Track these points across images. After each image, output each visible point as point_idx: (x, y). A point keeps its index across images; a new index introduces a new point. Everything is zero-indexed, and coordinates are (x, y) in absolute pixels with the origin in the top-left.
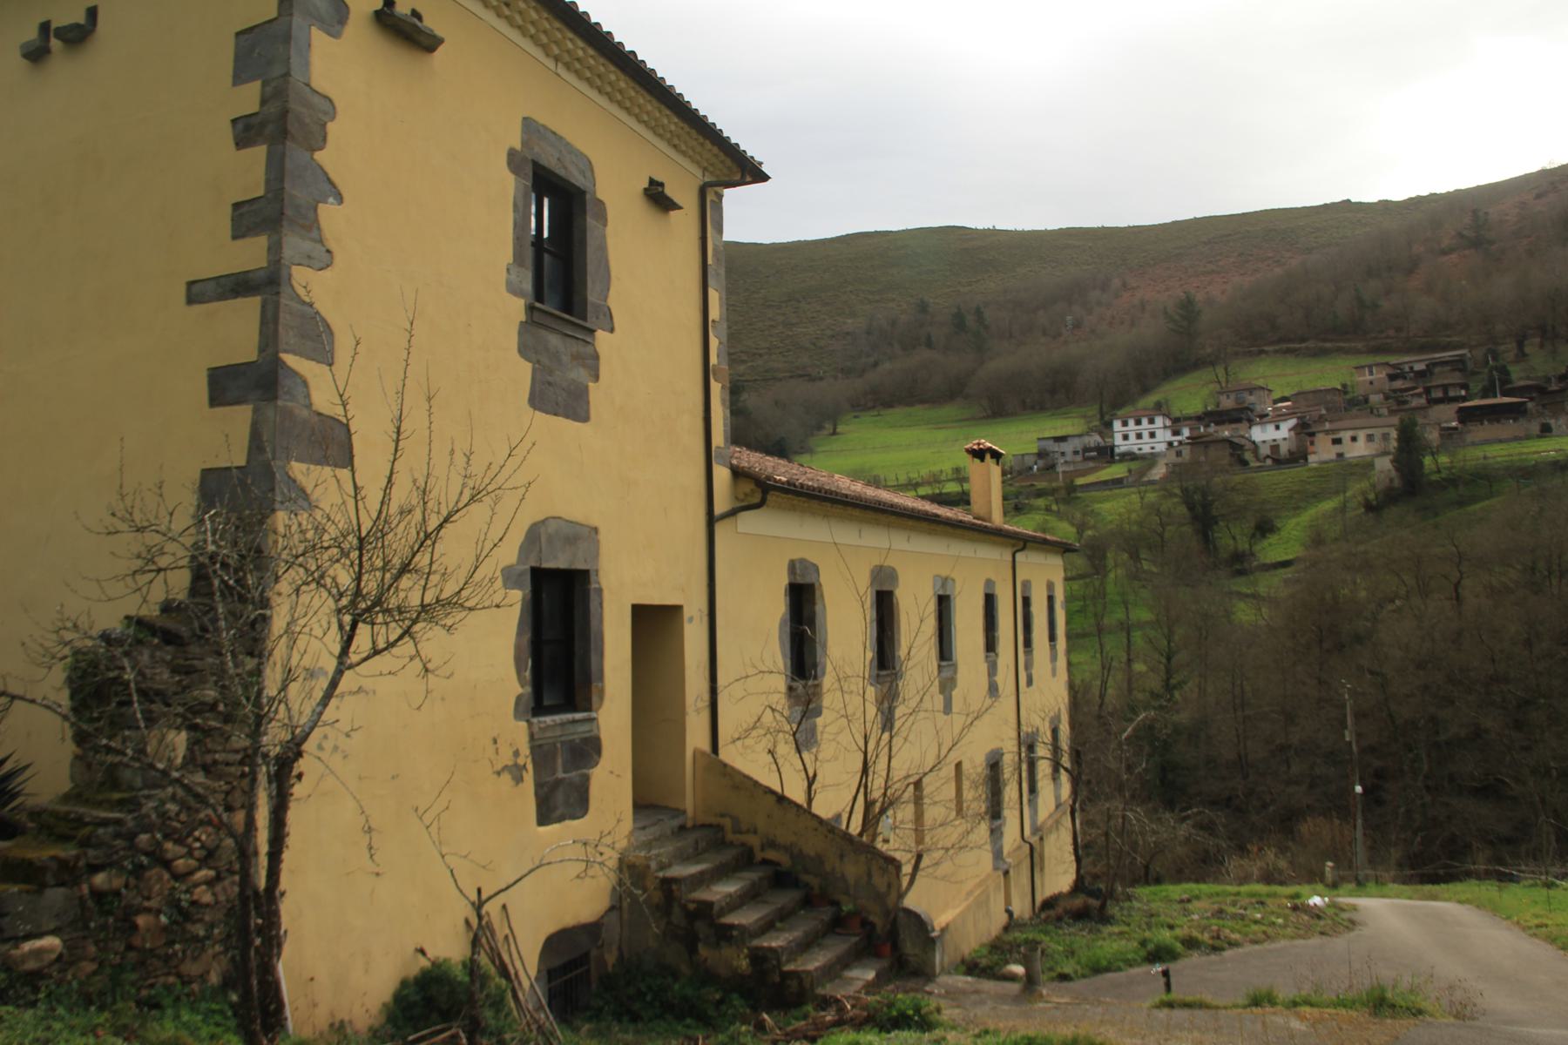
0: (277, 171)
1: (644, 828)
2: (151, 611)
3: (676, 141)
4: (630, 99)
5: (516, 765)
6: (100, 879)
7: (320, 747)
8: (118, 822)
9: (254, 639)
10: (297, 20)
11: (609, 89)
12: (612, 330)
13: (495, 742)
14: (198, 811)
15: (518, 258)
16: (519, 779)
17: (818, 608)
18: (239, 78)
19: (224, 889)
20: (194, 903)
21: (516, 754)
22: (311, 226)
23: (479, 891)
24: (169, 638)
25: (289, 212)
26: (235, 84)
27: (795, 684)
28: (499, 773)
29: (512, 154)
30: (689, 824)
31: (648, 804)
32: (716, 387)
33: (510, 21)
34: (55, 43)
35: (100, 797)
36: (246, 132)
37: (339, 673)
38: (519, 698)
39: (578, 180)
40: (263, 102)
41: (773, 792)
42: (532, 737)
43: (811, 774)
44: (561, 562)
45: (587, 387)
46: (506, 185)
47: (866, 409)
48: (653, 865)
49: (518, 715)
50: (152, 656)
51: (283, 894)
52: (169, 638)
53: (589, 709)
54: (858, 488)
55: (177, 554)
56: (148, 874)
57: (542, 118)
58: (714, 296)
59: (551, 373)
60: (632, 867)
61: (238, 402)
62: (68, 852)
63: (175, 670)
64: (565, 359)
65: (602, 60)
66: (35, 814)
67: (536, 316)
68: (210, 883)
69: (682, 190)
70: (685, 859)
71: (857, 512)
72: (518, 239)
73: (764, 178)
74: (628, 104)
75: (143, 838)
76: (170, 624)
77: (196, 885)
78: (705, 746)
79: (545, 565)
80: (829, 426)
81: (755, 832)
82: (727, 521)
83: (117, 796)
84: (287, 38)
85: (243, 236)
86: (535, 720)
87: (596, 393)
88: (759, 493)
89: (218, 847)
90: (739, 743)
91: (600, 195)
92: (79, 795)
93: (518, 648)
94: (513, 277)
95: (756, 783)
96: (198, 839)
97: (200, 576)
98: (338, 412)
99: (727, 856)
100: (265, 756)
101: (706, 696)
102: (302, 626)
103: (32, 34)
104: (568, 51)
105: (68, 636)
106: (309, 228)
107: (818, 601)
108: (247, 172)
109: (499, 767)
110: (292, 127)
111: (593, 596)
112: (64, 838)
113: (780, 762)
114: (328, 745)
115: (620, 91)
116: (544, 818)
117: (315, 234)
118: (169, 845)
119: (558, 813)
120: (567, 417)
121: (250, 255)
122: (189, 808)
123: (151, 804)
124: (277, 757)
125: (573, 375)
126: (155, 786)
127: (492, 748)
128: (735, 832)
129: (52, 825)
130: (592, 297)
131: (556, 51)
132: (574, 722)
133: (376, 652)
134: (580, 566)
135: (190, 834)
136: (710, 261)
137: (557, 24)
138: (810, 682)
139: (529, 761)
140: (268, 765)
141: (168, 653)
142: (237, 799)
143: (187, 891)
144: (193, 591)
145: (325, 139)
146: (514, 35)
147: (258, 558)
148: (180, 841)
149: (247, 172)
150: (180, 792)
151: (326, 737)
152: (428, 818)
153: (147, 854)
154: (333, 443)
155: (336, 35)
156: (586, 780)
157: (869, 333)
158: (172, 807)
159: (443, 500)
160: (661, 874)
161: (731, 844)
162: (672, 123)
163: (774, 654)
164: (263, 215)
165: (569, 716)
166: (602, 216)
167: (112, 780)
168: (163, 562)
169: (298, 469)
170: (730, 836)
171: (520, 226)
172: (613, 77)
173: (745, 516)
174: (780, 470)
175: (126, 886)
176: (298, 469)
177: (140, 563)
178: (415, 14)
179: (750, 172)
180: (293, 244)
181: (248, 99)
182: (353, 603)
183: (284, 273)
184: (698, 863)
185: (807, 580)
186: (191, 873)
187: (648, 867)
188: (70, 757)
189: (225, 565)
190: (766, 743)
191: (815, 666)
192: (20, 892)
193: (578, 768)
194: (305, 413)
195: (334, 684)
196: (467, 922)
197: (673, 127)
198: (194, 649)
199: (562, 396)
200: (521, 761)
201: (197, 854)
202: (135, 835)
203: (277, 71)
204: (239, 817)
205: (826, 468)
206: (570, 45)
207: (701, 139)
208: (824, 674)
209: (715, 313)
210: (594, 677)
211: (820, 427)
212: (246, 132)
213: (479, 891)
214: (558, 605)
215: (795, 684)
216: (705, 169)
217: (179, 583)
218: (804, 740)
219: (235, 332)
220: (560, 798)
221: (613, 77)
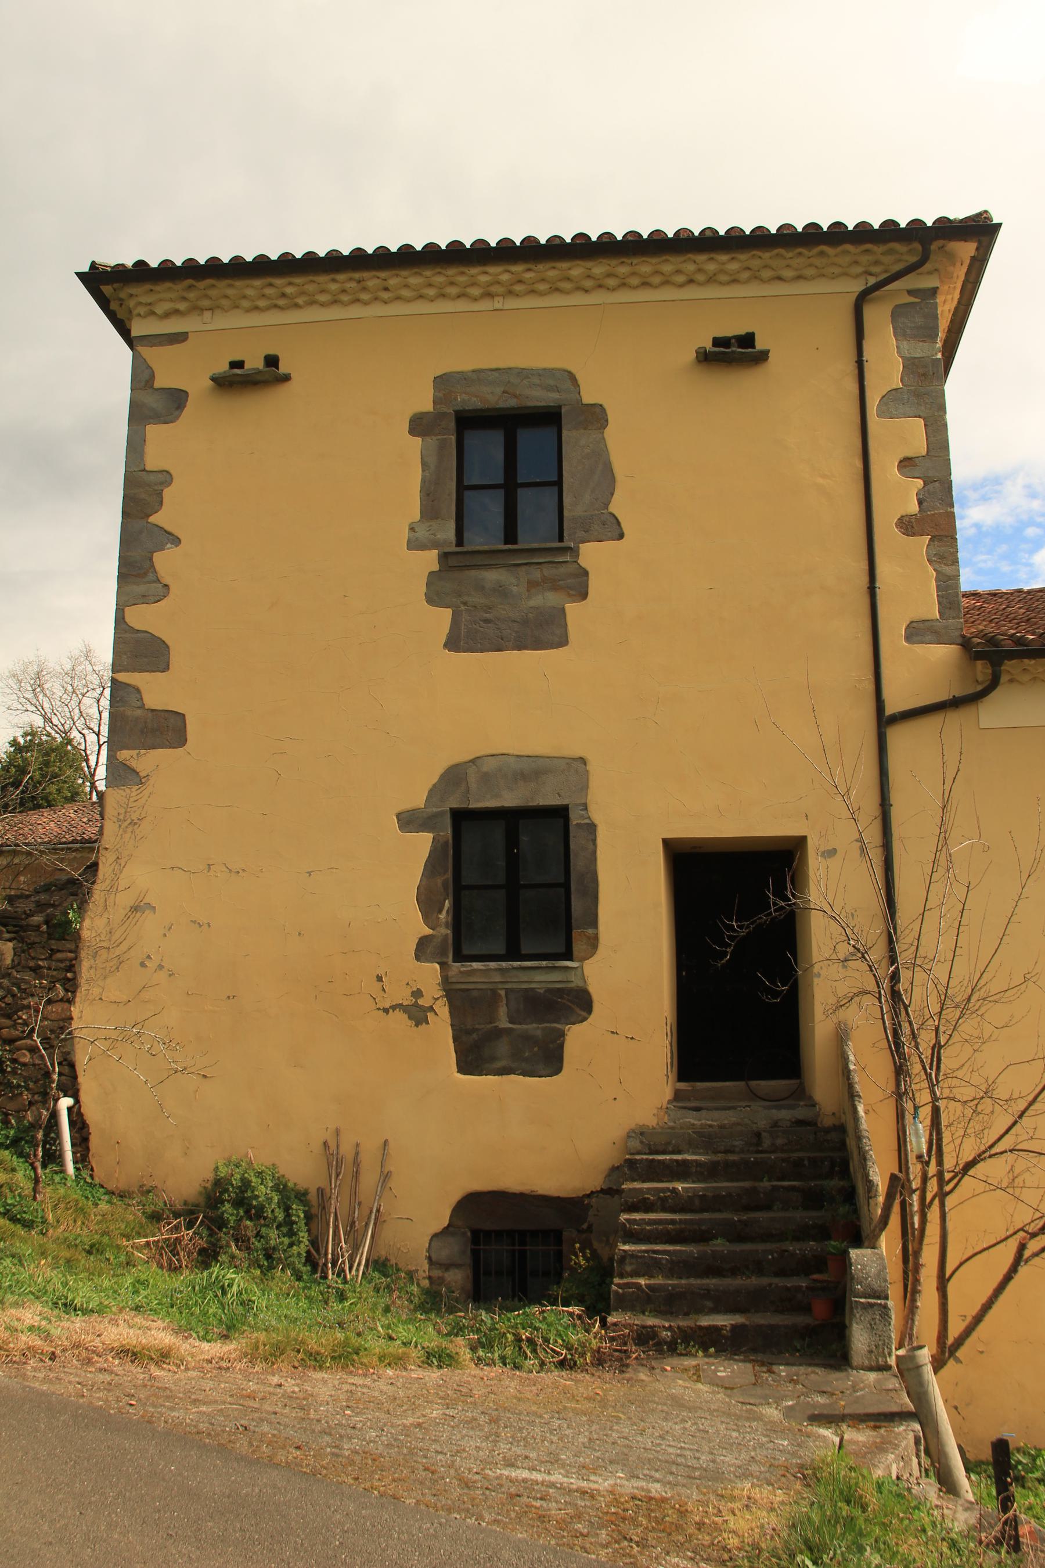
13: (380, 979)
15: (430, 511)
45: (563, 609)
77: (19, 1049)
79: (474, 805)
117: (151, 576)
135: (16, 1013)
156: (560, 1036)
194: (139, 712)
196: (325, 1143)
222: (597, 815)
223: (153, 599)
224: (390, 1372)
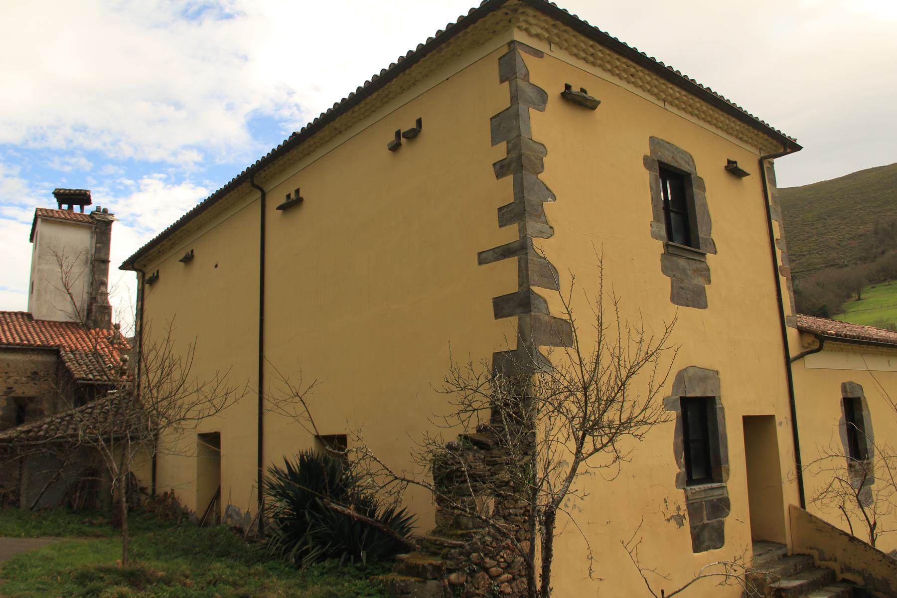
0: (519, 188)
1: (760, 555)
2: (472, 432)
3: (741, 135)
4: (710, 116)
5: (678, 515)
6: (453, 577)
7: (566, 506)
8: (461, 546)
9: (528, 448)
10: (521, 106)
11: (697, 112)
12: (716, 253)
14: (501, 541)
15: (656, 218)
16: (681, 524)
17: (864, 413)
18: (494, 141)
19: (517, 585)
20: (501, 592)
21: (679, 508)
22: (540, 215)
23: (663, 591)
24: (482, 446)
25: (527, 209)
26: (492, 145)
27: (853, 463)
28: (668, 520)
29: (645, 158)
30: (789, 554)
31: (761, 540)
32: (783, 280)
33: (635, 84)
34: (403, 140)
35: (451, 533)
36: (501, 169)
37: (576, 464)
38: (678, 475)
39: (686, 168)
40: (508, 152)
41: (846, 534)
42: (687, 498)
43: (872, 523)
44: (697, 393)
45: (704, 288)
46: (645, 177)
47: (880, 281)
48: (768, 579)
49: (678, 485)
50: (474, 456)
51: (551, 590)
52: (482, 446)
53: (722, 482)
54: (883, 334)
55: (482, 401)
56: (477, 575)
57: (660, 136)
58: (775, 224)
59: (682, 282)
60: (755, 579)
61: (510, 315)
62: (437, 561)
63: (489, 464)
64: (689, 272)
65: (691, 96)
66: (420, 541)
67: (671, 250)
68: (509, 582)
69: (748, 162)
70: (789, 576)
71: (885, 350)
72: (655, 207)
73: (799, 148)
74: (709, 119)
75: (474, 555)
76: (481, 438)
77: (502, 582)
78: (796, 503)
79: (688, 395)
80: (855, 296)
81: (836, 560)
82: (798, 361)
83: (460, 532)
84: (517, 116)
85: (505, 225)
86: (688, 488)
87: (709, 290)
88: (817, 342)
89: (513, 561)
90: (818, 502)
91: (699, 175)
92: (440, 531)
93: (675, 444)
94: (654, 229)
95: (833, 528)
96: (503, 557)
97: (495, 412)
98: (566, 317)
99: (817, 575)
100: (539, 511)
101: (795, 471)
102: (554, 439)
103: (392, 138)
104: (670, 95)
105: (431, 447)
106: (539, 216)
107: (864, 408)
108: (503, 191)
109: (668, 517)
110: (525, 162)
111: (719, 412)
112: (435, 554)
113: (849, 514)
114: (570, 504)
115: (704, 112)
116: (696, 549)
117: (543, 219)
118: (487, 560)
119: (706, 544)
120: (694, 307)
121: (510, 235)
122: (497, 540)
123: (478, 537)
124: (545, 512)
125: (695, 281)
126: (480, 527)
127: (663, 505)
128: (821, 560)
129: (429, 547)
130: (701, 235)
131: (663, 96)
132: (712, 488)
133: (596, 450)
134: (709, 394)
136: (770, 204)
137: (662, 81)
138: (865, 462)
139: (686, 512)
140: (539, 516)
141: (482, 454)
142: (522, 534)
143: (498, 586)
144: (493, 420)
145: (543, 166)
146: (638, 91)
147: (527, 400)
148: (492, 558)
149: (503, 191)
150: (492, 530)
151: (569, 500)
152: (630, 548)
153: (476, 564)
154: (564, 333)
155: (542, 110)
156: (722, 524)
157: (876, 233)
158: (488, 539)
159: (627, 360)
160: (776, 585)
161: (819, 567)
162: (737, 125)
163: (838, 444)
164: (515, 212)
165: (709, 485)
166: (703, 188)
167: (457, 524)
168: (475, 405)
169: (543, 349)
170: (818, 562)
171: (655, 199)
172: (698, 105)
173: (809, 357)
174: (829, 326)
175: (467, 582)
176: (543, 349)
177: (462, 407)
178: (583, 90)
179: (788, 146)
180: (532, 226)
181: (500, 152)
182: (583, 424)
183: (529, 242)
184: (797, 579)
185: (855, 395)
186: (499, 576)
187: (765, 580)
188: (434, 512)
189: (506, 405)
190: (838, 501)
191: (866, 451)
192: (415, 581)
193: (717, 517)
194: (547, 318)
195: (574, 470)
197: (738, 128)
198: (495, 452)
199: (689, 295)
200: (681, 513)
201: (502, 565)
202: (470, 554)
203: (514, 134)
204: (525, 545)
205: (856, 322)
206: (671, 91)
207: (756, 132)
208: (873, 456)
209: (777, 234)
210: (722, 462)
211: (849, 297)
212: (501, 169)
213: (663, 591)
214: (698, 418)
215: (853, 463)
216: (761, 149)
217: (485, 416)
218: (863, 500)
219: (505, 277)
220: (707, 536)
221: (698, 105)
222: (725, 404)
223: (546, 236)
224: (218, 565)
